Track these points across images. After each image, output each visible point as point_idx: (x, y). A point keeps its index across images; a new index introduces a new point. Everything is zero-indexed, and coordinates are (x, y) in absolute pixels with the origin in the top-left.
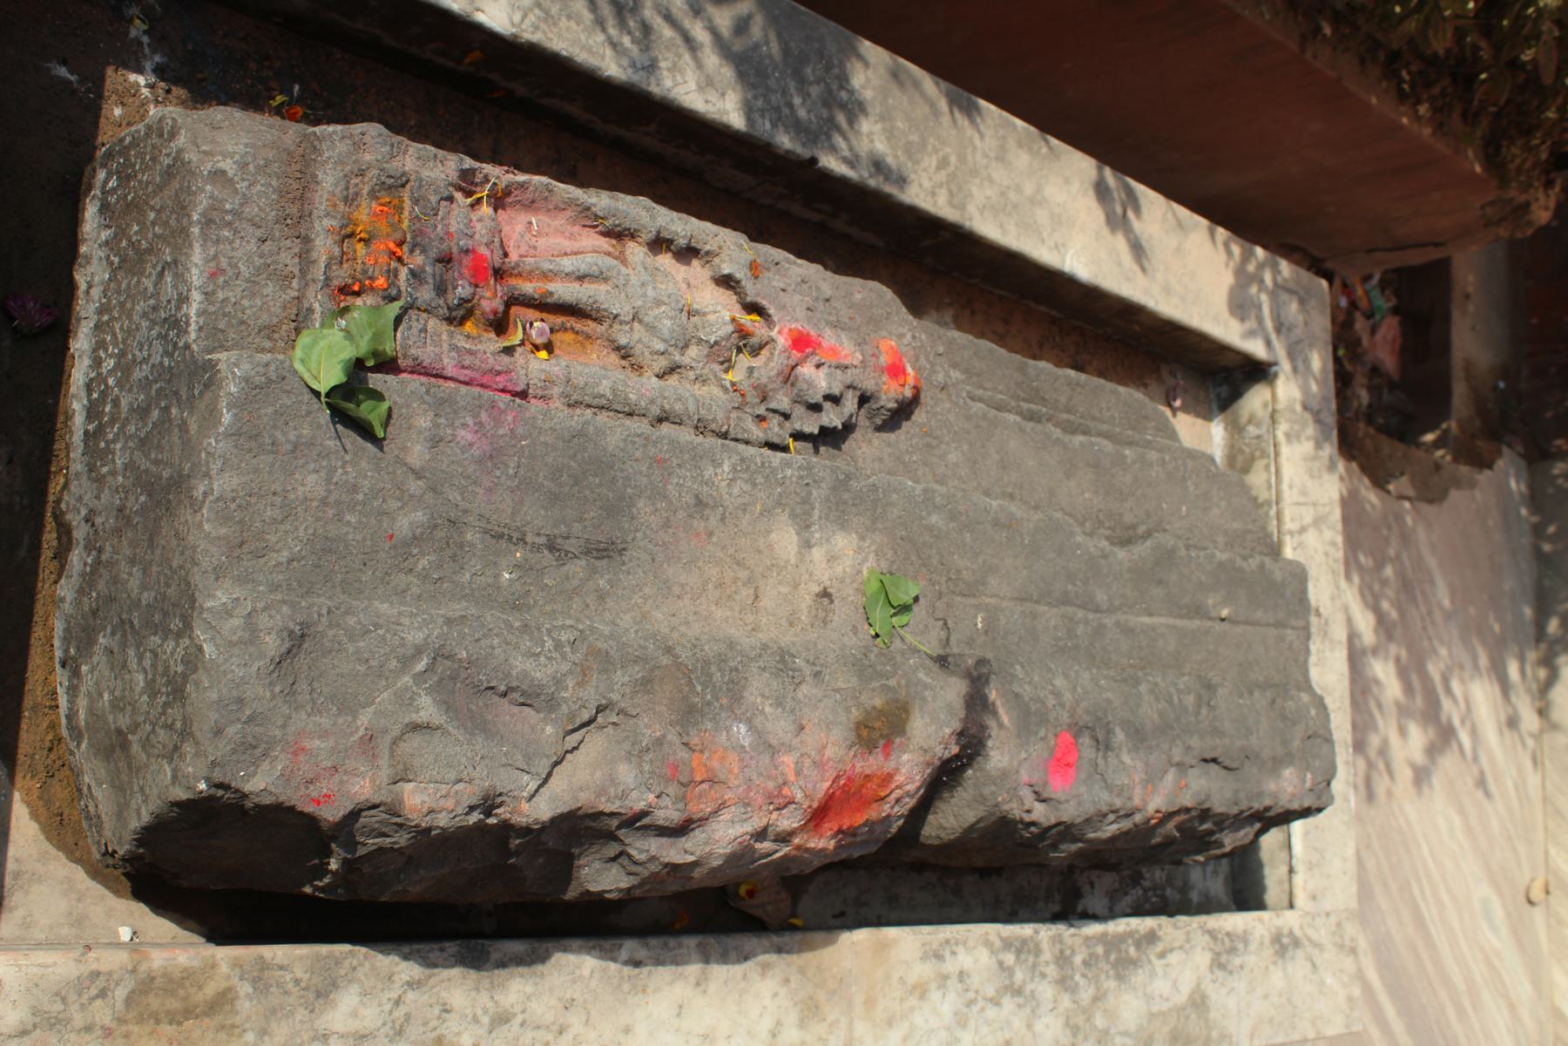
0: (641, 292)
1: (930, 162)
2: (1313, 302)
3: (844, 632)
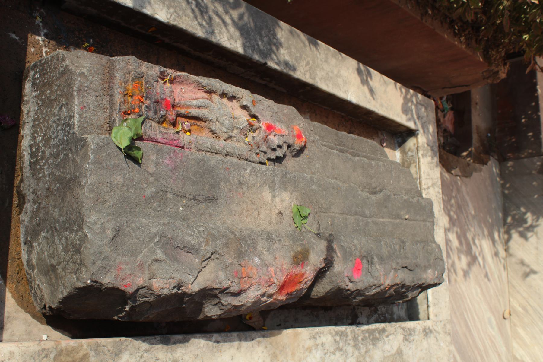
0: (218, 111)
1: (303, 63)
2: (429, 109)
3: (286, 225)
